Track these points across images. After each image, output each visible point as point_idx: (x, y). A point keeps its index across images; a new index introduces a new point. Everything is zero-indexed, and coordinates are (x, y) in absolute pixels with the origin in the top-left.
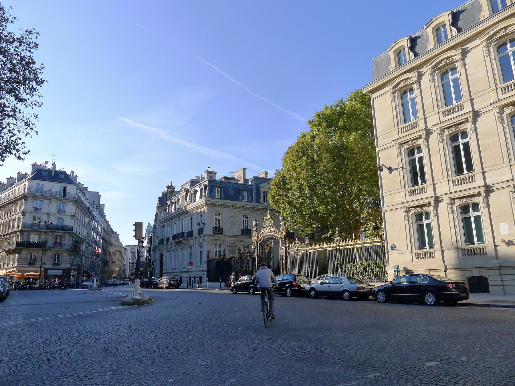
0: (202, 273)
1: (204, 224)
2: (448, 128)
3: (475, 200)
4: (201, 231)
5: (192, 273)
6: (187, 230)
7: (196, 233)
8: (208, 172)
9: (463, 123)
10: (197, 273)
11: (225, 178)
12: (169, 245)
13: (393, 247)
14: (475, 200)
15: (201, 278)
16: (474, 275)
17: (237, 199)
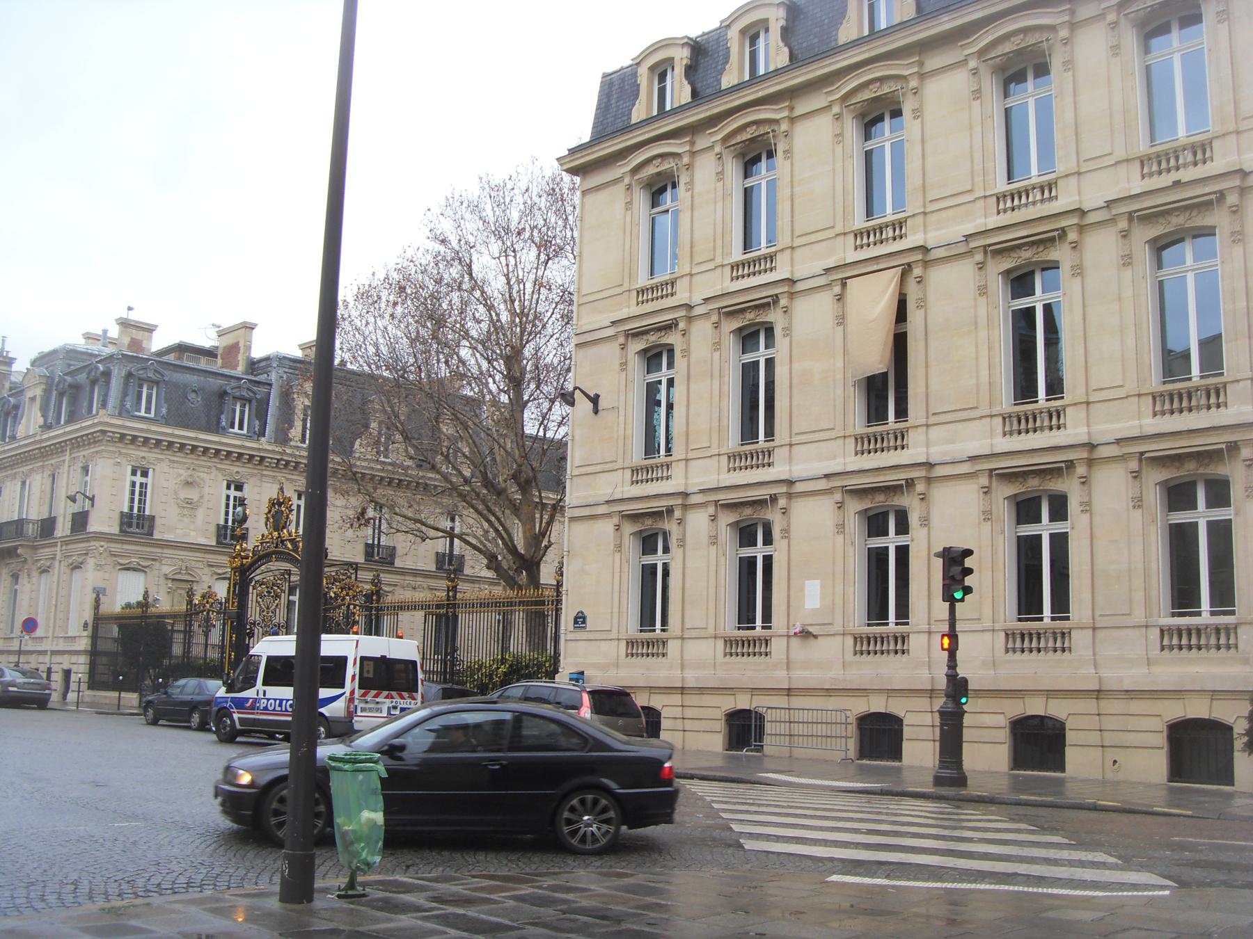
0: (74, 659)
1: (92, 499)
2: (731, 314)
3: (1057, 485)
4: (80, 521)
5: (41, 658)
6: (36, 512)
7: (63, 528)
8: (125, 324)
9: (1209, 204)
10: (58, 659)
11: (182, 349)
12: (55, 545)
13: (580, 620)
14: (1057, 485)
15: (67, 674)
16: (872, 710)
17: (216, 428)
